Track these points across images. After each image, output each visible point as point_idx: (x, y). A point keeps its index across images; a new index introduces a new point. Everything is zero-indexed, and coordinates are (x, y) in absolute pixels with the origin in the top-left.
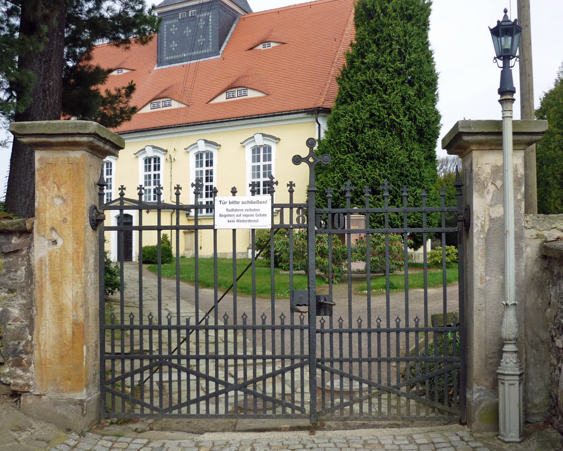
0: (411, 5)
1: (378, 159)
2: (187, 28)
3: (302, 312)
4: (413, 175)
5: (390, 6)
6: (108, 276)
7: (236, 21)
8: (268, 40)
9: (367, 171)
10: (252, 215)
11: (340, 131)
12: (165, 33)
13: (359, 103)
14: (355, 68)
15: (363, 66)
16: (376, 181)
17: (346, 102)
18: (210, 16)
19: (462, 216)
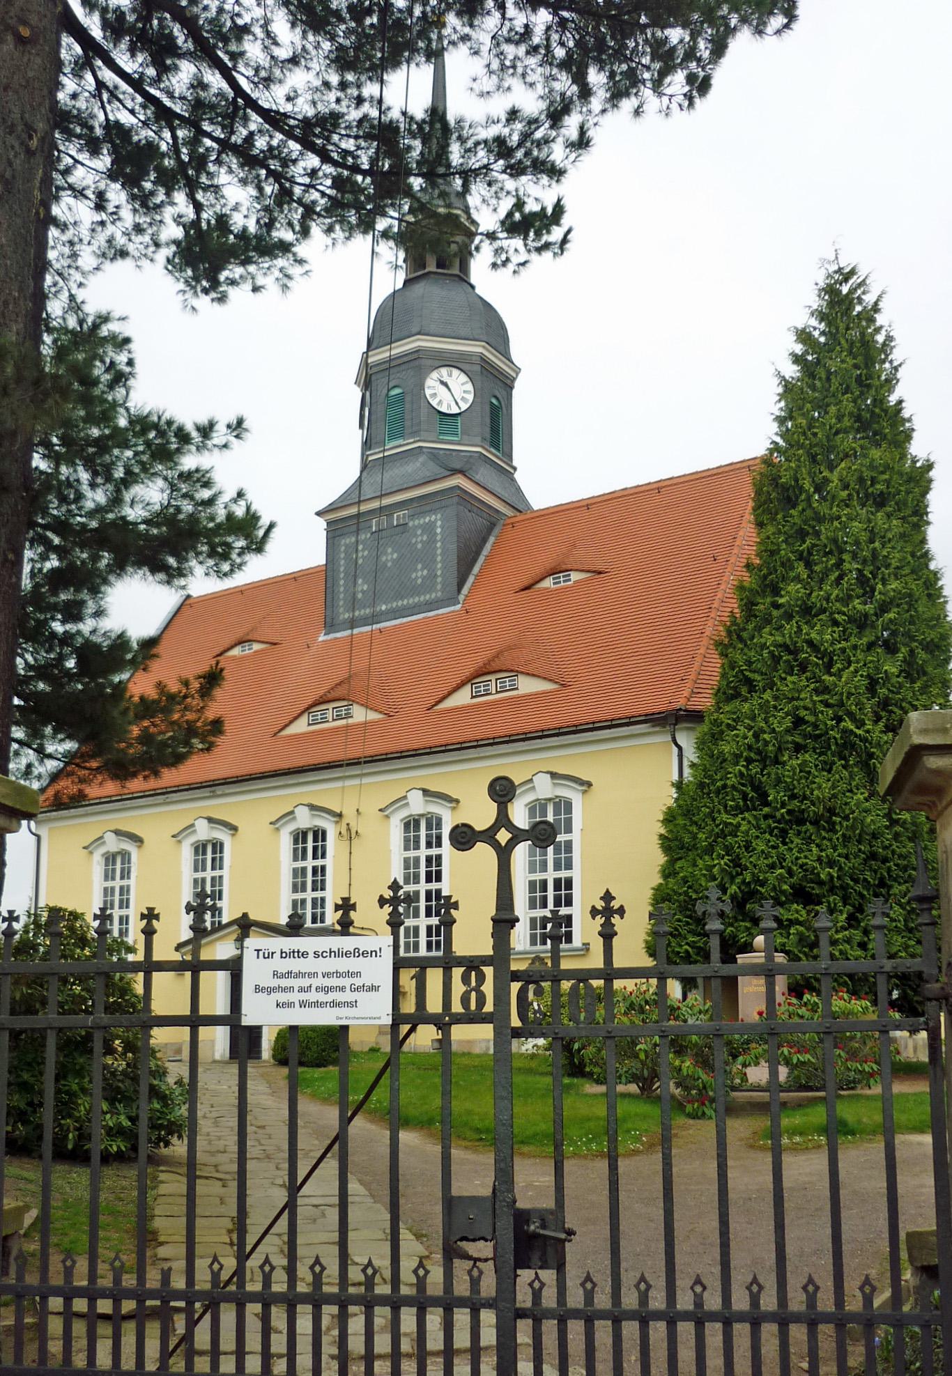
0: (883, 473)
1: (815, 823)
2: (390, 550)
3: (476, 1260)
4: (900, 856)
5: (835, 477)
6: (157, 1106)
7: (496, 531)
8: (564, 567)
9: (791, 850)
10: (342, 989)
11: (725, 760)
12: (342, 562)
13: (767, 696)
14: (756, 617)
15: (775, 613)
16: (812, 873)
17: (737, 695)
18: (439, 523)
19: (938, 985)
